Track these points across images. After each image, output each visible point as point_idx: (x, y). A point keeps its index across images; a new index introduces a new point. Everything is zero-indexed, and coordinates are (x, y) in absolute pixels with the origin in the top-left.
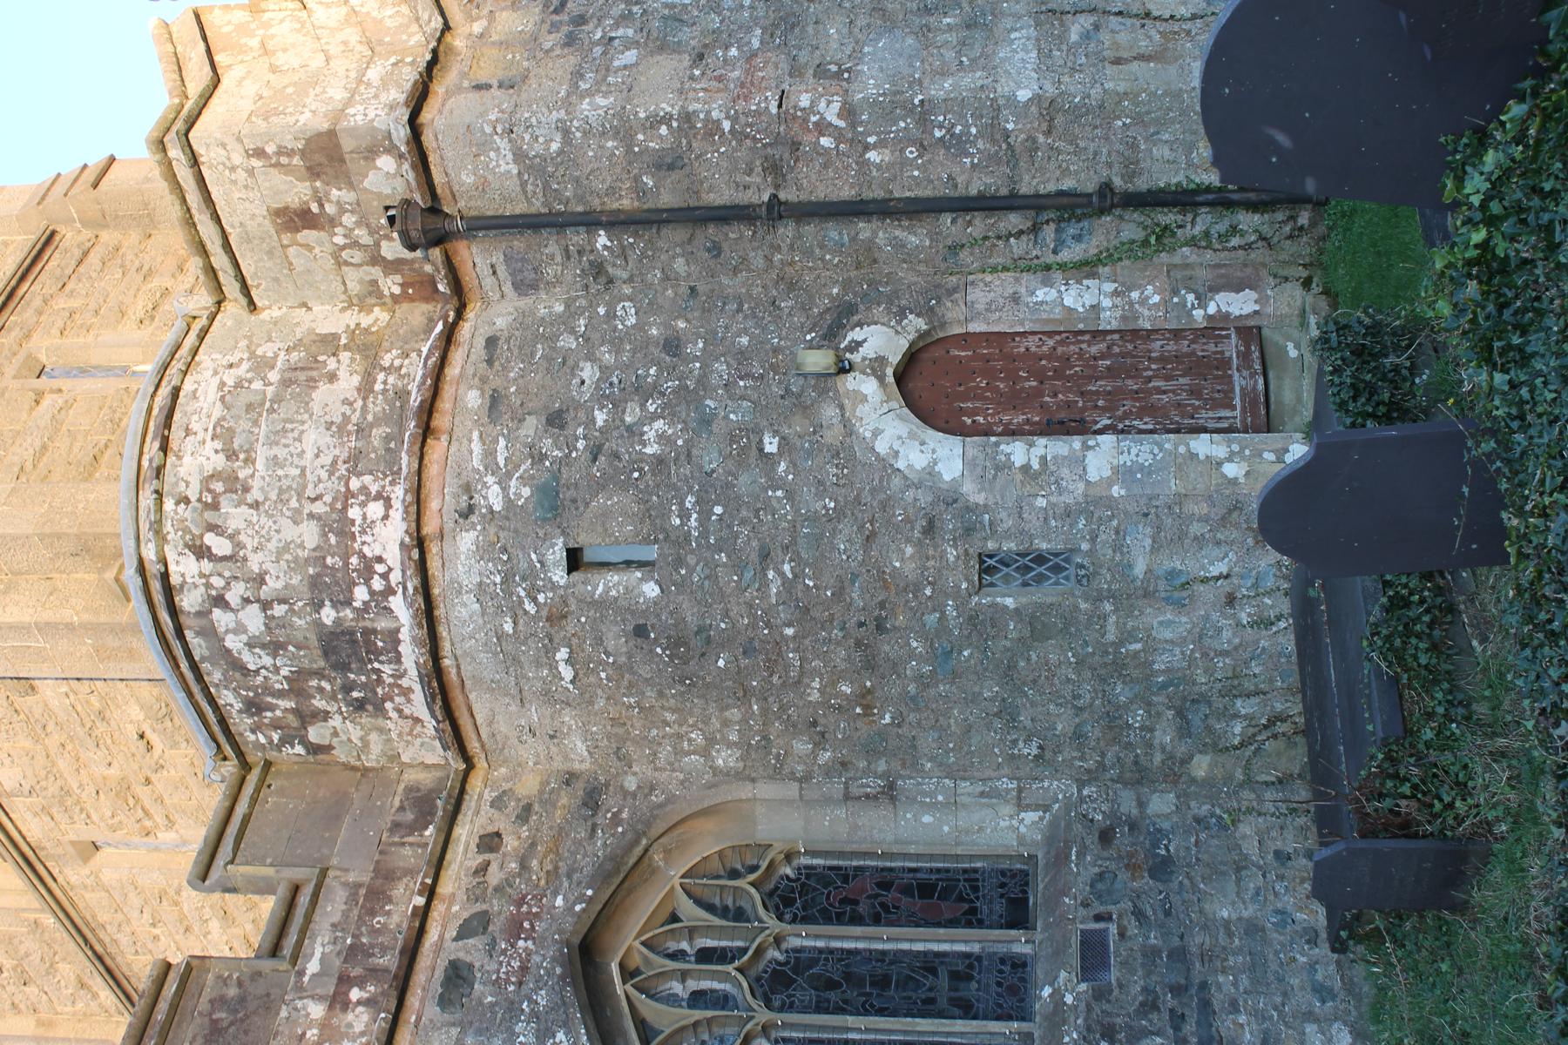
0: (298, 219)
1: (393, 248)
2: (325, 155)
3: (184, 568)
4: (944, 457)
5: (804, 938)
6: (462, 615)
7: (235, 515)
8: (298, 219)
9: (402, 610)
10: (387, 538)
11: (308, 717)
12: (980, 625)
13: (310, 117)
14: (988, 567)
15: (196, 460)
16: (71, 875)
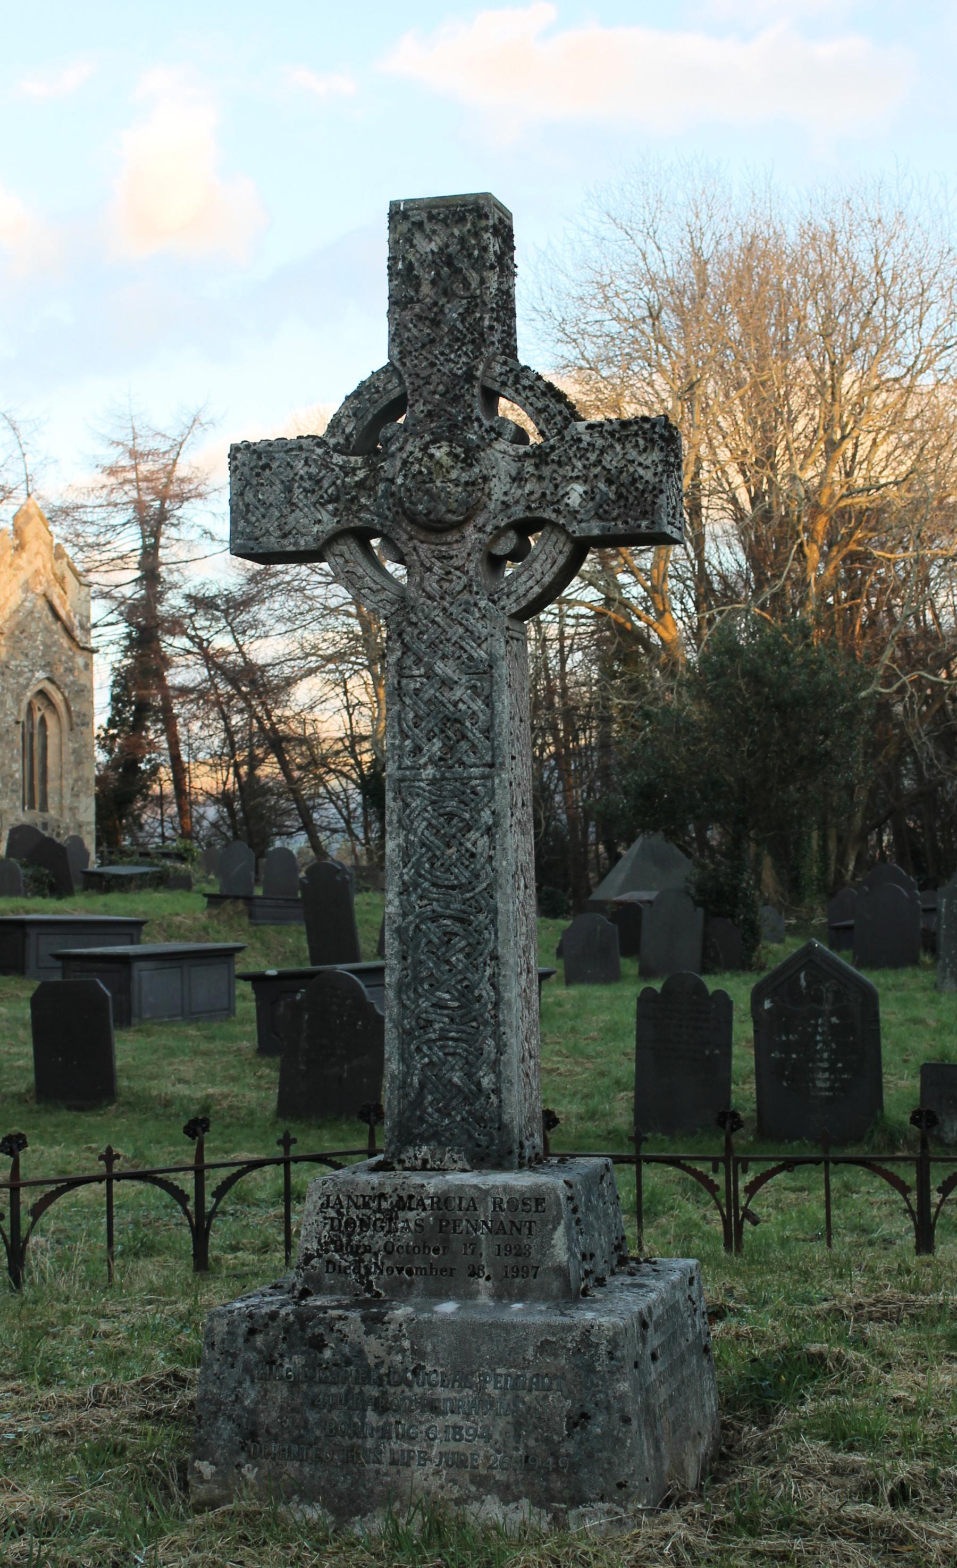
5: (37, 806)
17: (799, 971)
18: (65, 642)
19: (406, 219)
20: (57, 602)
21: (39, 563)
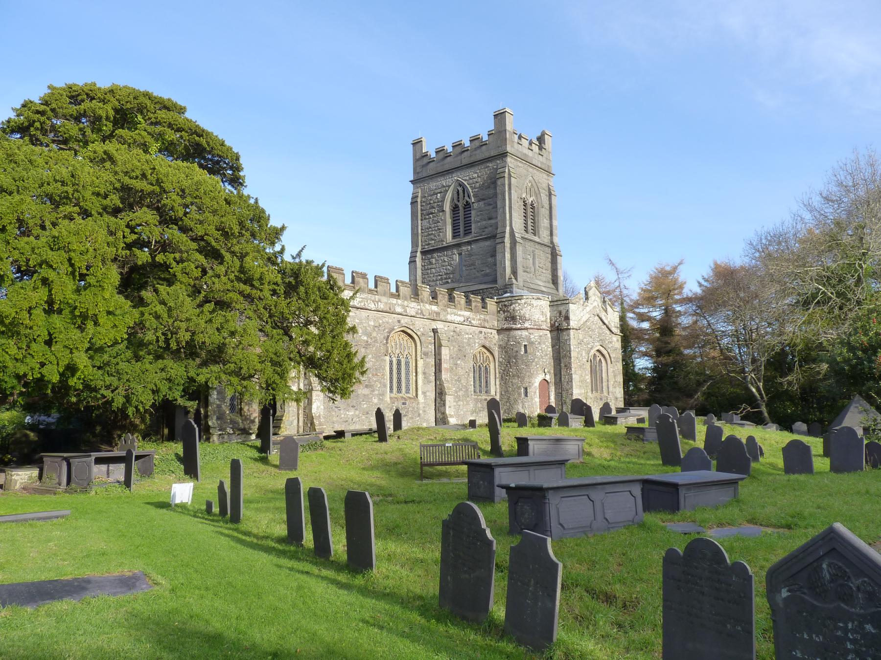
0: (560, 313)
1: (557, 324)
2: (567, 318)
3: (523, 301)
4: (537, 384)
6: (519, 332)
7: (529, 308)
8: (560, 313)
9: (519, 326)
10: (527, 325)
11: (504, 312)
12: (519, 388)
13: (571, 316)
14: (526, 389)
15: (534, 302)
16: (455, 251)
17: (821, 559)
18: (608, 332)
19: (428, 169)
20: (604, 318)
21: (595, 304)
